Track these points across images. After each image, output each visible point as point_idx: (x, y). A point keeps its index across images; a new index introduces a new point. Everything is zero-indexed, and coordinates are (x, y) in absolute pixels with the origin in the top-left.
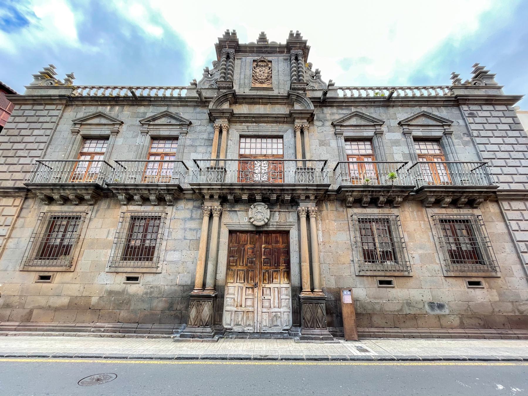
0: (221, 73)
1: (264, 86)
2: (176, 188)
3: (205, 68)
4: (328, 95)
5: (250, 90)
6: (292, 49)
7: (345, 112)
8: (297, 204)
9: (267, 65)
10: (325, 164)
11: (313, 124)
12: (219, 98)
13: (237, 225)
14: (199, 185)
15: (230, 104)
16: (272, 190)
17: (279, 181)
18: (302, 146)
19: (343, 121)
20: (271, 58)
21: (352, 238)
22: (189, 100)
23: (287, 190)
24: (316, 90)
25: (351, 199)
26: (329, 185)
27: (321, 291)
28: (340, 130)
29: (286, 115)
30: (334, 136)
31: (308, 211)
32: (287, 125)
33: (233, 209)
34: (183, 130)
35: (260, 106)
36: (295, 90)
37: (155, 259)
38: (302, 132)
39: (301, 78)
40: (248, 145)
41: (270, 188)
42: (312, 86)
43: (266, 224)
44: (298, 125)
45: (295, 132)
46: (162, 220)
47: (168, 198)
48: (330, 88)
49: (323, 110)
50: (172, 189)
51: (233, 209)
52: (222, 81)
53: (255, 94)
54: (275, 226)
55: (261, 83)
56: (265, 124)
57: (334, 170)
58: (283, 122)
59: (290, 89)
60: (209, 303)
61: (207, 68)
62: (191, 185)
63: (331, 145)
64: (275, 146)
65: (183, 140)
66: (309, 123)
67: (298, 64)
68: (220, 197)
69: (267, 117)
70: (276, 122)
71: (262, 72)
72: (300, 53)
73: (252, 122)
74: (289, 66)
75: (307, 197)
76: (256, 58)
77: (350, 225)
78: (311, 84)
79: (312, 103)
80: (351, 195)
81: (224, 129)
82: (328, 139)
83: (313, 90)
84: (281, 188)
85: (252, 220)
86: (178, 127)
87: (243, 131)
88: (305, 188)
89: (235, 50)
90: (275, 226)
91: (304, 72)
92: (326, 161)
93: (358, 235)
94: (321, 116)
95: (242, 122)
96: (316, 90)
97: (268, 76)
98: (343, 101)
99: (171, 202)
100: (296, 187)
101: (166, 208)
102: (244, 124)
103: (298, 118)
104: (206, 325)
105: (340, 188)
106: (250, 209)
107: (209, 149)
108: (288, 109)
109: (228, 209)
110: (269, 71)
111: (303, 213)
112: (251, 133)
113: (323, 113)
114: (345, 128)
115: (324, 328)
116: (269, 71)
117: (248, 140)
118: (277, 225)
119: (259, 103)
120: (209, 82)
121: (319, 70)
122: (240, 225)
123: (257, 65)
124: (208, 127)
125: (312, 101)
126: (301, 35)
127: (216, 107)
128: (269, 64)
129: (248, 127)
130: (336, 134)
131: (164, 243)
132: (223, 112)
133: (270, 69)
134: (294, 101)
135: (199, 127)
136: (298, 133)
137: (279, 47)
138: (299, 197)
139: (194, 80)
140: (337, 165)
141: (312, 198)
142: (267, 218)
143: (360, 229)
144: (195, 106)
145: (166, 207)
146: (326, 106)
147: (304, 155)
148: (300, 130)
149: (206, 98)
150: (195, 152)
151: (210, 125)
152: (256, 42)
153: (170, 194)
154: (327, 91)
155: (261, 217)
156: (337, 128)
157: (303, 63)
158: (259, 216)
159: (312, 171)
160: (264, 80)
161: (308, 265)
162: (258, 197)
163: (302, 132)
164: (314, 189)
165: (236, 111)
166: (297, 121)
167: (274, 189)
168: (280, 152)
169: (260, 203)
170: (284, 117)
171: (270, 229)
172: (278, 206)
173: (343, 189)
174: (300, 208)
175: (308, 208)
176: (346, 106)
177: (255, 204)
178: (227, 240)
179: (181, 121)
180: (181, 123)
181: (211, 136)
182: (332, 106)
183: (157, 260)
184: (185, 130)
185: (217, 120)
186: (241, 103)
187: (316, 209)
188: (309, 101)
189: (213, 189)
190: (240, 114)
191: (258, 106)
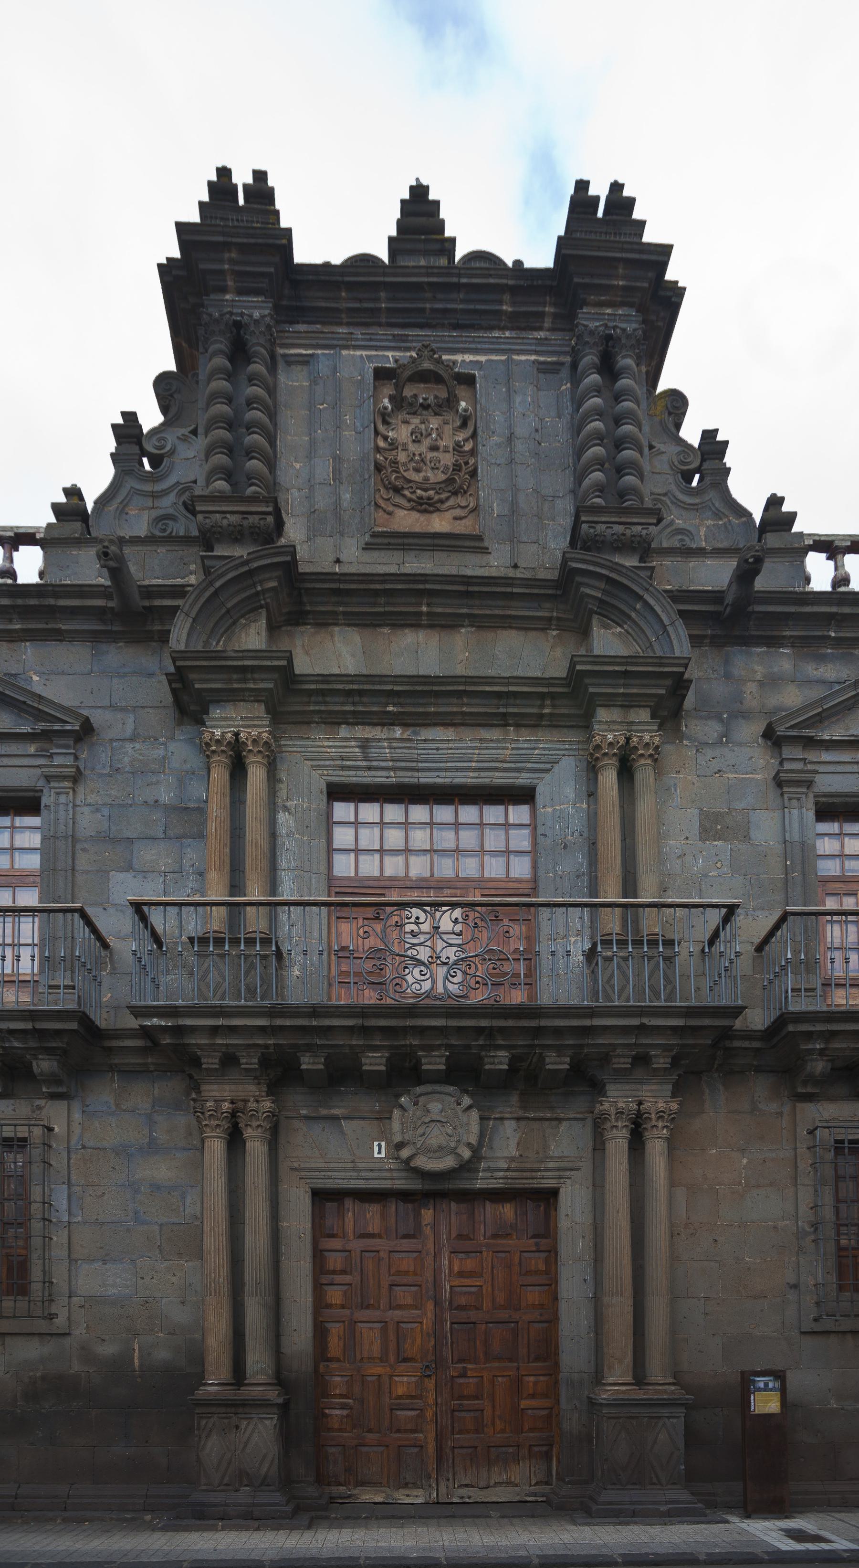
0: (209, 452)
1: (440, 523)
2: (74, 1026)
3: (120, 420)
4: (760, 584)
5: (368, 547)
6: (584, 303)
7: (830, 671)
8: (597, 1088)
9: (450, 403)
10: (726, 920)
11: (677, 730)
12: (216, 593)
13: (345, 1170)
14: (172, 1012)
15: (273, 628)
16: (490, 1032)
17: (517, 997)
18: (624, 840)
19: (820, 719)
20: (468, 358)
21: (803, 1208)
22: (62, 602)
23: (558, 1032)
24: (700, 552)
25: (819, 1066)
26: (737, 1011)
27: (672, 1380)
28: (799, 766)
29: (548, 682)
30: (772, 793)
31: (639, 1114)
32: (556, 735)
33: (324, 1112)
34: (57, 761)
35: (422, 635)
36: (599, 550)
37: (36, 1288)
38: (626, 772)
39: (630, 479)
40: (369, 838)
41: (484, 1023)
42: (680, 531)
43: (466, 1168)
44: (610, 737)
45: (592, 770)
46: (36, 1153)
47: (44, 1065)
48: (772, 540)
49: (727, 662)
50: (58, 1032)
51: (324, 1112)
52: (221, 498)
53: (393, 569)
54: (501, 1174)
55: (425, 506)
56: (448, 733)
57: (760, 948)
58: (536, 722)
59: (573, 543)
60: (267, 1422)
61: (130, 417)
62: (138, 1012)
63: (753, 834)
64: (493, 840)
65: (62, 813)
66: (661, 727)
67: (618, 398)
68: (265, 1062)
69: (460, 694)
70: (503, 721)
71: (427, 442)
72: (629, 328)
73: (387, 721)
74: (568, 409)
75: (642, 1060)
76: (390, 357)
77: (801, 1166)
78: (677, 519)
79: (679, 623)
80: (822, 1052)
81: (252, 758)
82: (742, 805)
83: (688, 552)
84: (534, 1023)
85: (405, 1153)
86: (32, 749)
87: (343, 768)
88: (635, 1022)
89: (276, 308)
90: (501, 1174)
91: (646, 450)
92: (731, 910)
93: (828, 1198)
94: (719, 690)
95: (334, 720)
96: (700, 552)
97: (457, 468)
98: (831, 616)
99: (59, 1082)
100: (597, 1022)
101: (39, 1108)
102: (344, 731)
103: (609, 701)
104: (262, 1484)
105: (783, 1020)
106: (397, 1113)
107: (191, 855)
108: (558, 652)
109: (304, 1112)
110: (460, 437)
111: (620, 1124)
112: (380, 778)
113: (728, 676)
114: (826, 756)
115: (674, 1484)
116: (460, 437)
117: (369, 811)
118: (508, 1170)
119: (413, 622)
120: (149, 502)
121: (720, 437)
122: (359, 1171)
123: (398, 402)
124: (172, 746)
125: (681, 613)
126: (637, 214)
127: (206, 643)
128: (461, 391)
129: (365, 744)
130: (779, 783)
131: (59, 1237)
132: (244, 669)
133: (464, 425)
134: (592, 612)
135: (129, 746)
136: (609, 778)
137: (513, 290)
138: (605, 1059)
139: (68, 492)
140: (777, 927)
141: (661, 1062)
142: (469, 1145)
143: (838, 1178)
144: (95, 638)
145: (42, 1102)
146: (746, 641)
147: (629, 885)
148: (614, 761)
149: (149, 592)
150: (129, 867)
151: (178, 735)
152: (383, 253)
153: (49, 1051)
154: (759, 561)
155: (442, 1141)
156: (787, 752)
157: (640, 391)
158: (436, 1137)
159: (669, 953)
160: (438, 487)
161: (630, 1302)
162: (434, 1062)
163: (626, 772)
164: (674, 1029)
165: (302, 665)
166: (602, 714)
167: (501, 1030)
168: (521, 868)
169: (437, 1087)
170: (542, 696)
171: (479, 1184)
172: (514, 1099)
173: (791, 1028)
174: (606, 1105)
175: (640, 1103)
176: (839, 642)
177: (419, 1090)
178: (308, 1226)
179: (39, 715)
180: (42, 726)
181: (196, 790)
182: (772, 642)
183: (47, 1294)
184: (62, 761)
185: (216, 712)
186: (324, 622)
187: (674, 1106)
188: (666, 612)
189: (232, 1029)
190: (326, 678)
191: (409, 638)
